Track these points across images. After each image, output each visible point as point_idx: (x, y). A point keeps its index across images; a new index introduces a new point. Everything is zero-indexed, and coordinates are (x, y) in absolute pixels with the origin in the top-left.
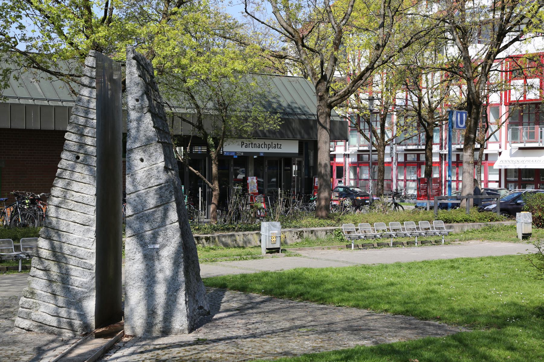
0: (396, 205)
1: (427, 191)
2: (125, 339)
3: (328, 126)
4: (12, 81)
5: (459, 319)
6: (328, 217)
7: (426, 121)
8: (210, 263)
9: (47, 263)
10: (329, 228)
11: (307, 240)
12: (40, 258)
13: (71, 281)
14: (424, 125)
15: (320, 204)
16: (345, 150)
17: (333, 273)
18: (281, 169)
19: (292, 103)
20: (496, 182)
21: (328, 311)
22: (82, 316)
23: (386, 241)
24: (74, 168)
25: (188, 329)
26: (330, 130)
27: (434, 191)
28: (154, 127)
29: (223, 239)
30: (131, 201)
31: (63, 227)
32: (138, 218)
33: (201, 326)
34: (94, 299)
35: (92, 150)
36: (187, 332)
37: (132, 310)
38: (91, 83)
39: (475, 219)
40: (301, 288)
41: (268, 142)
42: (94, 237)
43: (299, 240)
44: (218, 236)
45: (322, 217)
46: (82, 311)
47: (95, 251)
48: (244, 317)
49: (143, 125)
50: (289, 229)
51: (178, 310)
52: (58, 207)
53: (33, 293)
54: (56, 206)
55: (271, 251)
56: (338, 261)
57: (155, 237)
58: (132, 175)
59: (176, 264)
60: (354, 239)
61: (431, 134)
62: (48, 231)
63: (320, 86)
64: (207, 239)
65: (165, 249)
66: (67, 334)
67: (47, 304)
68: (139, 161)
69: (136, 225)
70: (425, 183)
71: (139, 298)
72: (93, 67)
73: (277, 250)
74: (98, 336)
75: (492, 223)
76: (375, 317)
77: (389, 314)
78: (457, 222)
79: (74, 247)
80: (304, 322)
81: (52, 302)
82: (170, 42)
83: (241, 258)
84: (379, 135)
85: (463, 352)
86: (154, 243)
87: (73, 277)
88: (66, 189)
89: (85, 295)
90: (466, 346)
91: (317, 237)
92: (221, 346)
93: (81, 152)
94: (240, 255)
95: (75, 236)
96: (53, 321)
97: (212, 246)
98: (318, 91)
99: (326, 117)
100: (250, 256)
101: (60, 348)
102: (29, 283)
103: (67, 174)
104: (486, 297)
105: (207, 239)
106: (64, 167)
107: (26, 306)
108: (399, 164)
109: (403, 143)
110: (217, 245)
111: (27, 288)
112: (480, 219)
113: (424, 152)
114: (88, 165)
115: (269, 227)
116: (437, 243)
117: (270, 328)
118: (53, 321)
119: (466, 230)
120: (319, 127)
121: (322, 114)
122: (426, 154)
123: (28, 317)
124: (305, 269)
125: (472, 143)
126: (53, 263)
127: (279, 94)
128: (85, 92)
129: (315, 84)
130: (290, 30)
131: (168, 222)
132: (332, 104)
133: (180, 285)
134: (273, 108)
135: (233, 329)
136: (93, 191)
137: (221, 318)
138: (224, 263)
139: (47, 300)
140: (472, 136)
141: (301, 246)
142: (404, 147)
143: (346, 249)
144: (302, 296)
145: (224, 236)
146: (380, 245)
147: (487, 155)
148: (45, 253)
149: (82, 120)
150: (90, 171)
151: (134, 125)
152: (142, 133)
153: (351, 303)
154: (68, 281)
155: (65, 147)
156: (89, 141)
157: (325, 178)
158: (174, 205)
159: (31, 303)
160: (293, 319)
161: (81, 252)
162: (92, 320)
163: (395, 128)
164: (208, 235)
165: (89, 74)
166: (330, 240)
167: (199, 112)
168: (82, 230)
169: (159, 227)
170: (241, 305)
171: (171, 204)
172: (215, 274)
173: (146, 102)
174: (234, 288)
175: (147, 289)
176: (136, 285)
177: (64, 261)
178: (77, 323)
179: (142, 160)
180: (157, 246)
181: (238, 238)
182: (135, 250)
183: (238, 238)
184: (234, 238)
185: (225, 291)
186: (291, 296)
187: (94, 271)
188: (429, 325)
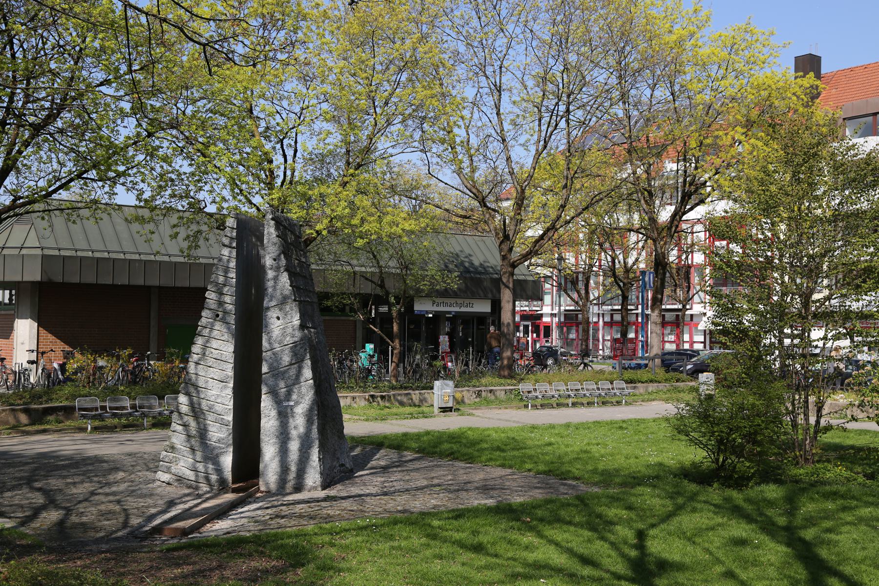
0: (586, 365)
1: (622, 352)
2: (259, 495)
3: (511, 285)
4: (201, 242)
5: (597, 478)
6: (511, 377)
7: (621, 281)
8: (379, 421)
9: (186, 418)
10: (508, 388)
11: (485, 400)
12: (180, 413)
13: (209, 436)
14: (619, 286)
15: (502, 363)
16: (552, 310)
17: (496, 432)
18: (473, 329)
19: (484, 262)
20: (702, 342)
21: (473, 470)
22: (219, 471)
23: (566, 401)
24: (213, 326)
25: (322, 486)
26: (513, 289)
27: (630, 351)
28: (290, 286)
29: (399, 398)
30: (268, 358)
31: (201, 383)
32: (273, 376)
33: (339, 483)
34: (231, 454)
35: (230, 307)
36: (320, 489)
37: (266, 466)
38: (231, 243)
39: (660, 380)
40: (455, 447)
41: (460, 301)
42: (231, 393)
43: (478, 400)
44: (394, 395)
45: (504, 377)
46: (219, 466)
47: (232, 407)
48: (386, 475)
49: (280, 284)
50: (467, 388)
51: (312, 466)
52: (197, 363)
53: (173, 448)
54: (196, 363)
55: (445, 410)
56: (509, 421)
57: (289, 394)
58: (269, 333)
59: (309, 421)
60: (531, 399)
61: (627, 294)
62: (187, 386)
63: (503, 246)
64: (383, 397)
65: (299, 406)
66: (204, 488)
67: (186, 459)
68: (276, 320)
69: (271, 382)
70: (621, 343)
71: (273, 454)
72: (233, 228)
73: (450, 409)
74: (234, 491)
75: (678, 384)
76: (516, 477)
77: (531, 473)
78: (642, 382)
79: (212, 403)
80: (442, 481)
81: (191, 457)
82: (341, 203)
83: (412, 416)
84: (583, 295)
85: (580, 511)
86: (288, 401)
87: (210, 433)
88: (205, 347)
89: (223, 451)
90: (586, 505)
91: (496, 397)
92: (346, 504)
93: (220, 310)
94: (411, 414)
95: (214, 392)
96: (190, 475)
97: (387, 405)
98: (501, 250)
99: (509, 276)
100: (421, 415)
101: (192, 502)
102: (169, 437)
103: (206, 332)
104: (637, 458)
105: (383, 397)
106: (204, 325)
107: (166, 460)
108: (605, 323)
109: (607, 303)
110: (392, 404)
111: (167, 443)
112: (666, 380)
113: (7, 301)
114: (227, 323)
115: (442, 385)
116: (619, 403)
117: (406, 487)
118: (190, 475)
119: (650, 391)
120: (502, 287)
121: (505, 273)
122: (622, 314)
123: (168, 471)
124: (470, 429)
125: (659, 304)
126: (192, 418)
127: (472, 253)
128: (226, 252)
129: (498, 244)
130: (474, 190)
131: (302, 379)
132: (516, 264)
133: (312, 442)
134: (465, 267)
135: (369, 487)
136: (231, 348)
137: (362, 476)
138: (394, 422)
139: (186, 455)
140: (660, 296)
141: (477, 406)
142: (610, 307)
143: (523, 409)
144: (453, 456)
145: (399, 395)
146: (559, 405)
147: (692, 316)
148: (184, 409)
149: (221, 279)
150: (229, 329)
151: (270, 284)
152: (278, 293)
153: (498, 463)
154: (206, 437)
155: (205, 306)
156: (228, 299)
157: (508, 337)
158: (309, 362)
159: (171, 457)
160: (433, 478)
161: (218, 408)
162: (228, 474)
163: (601, 288)
164: (384, 394)
165: (229, 235)
166: (509, 400)
167: (381, 272)
168: (221, 386)
169: (294, 384)
170: (389, 463)
171: (306, 362)
172: (380, 432)
173: (283, 262)
174: (391, 447)
175: (281, 446)
176: (271, 441)
177: (202, 416)
178: (214, 477)
179: (278, 318)
180: (292, 403)
181: (414, 397)
182: (270, 407)
183: (414, 396)
184: (410, 397)
185: (381, 449)
186: (442, 455)
187: (231, 427)
188: (565, 485)
